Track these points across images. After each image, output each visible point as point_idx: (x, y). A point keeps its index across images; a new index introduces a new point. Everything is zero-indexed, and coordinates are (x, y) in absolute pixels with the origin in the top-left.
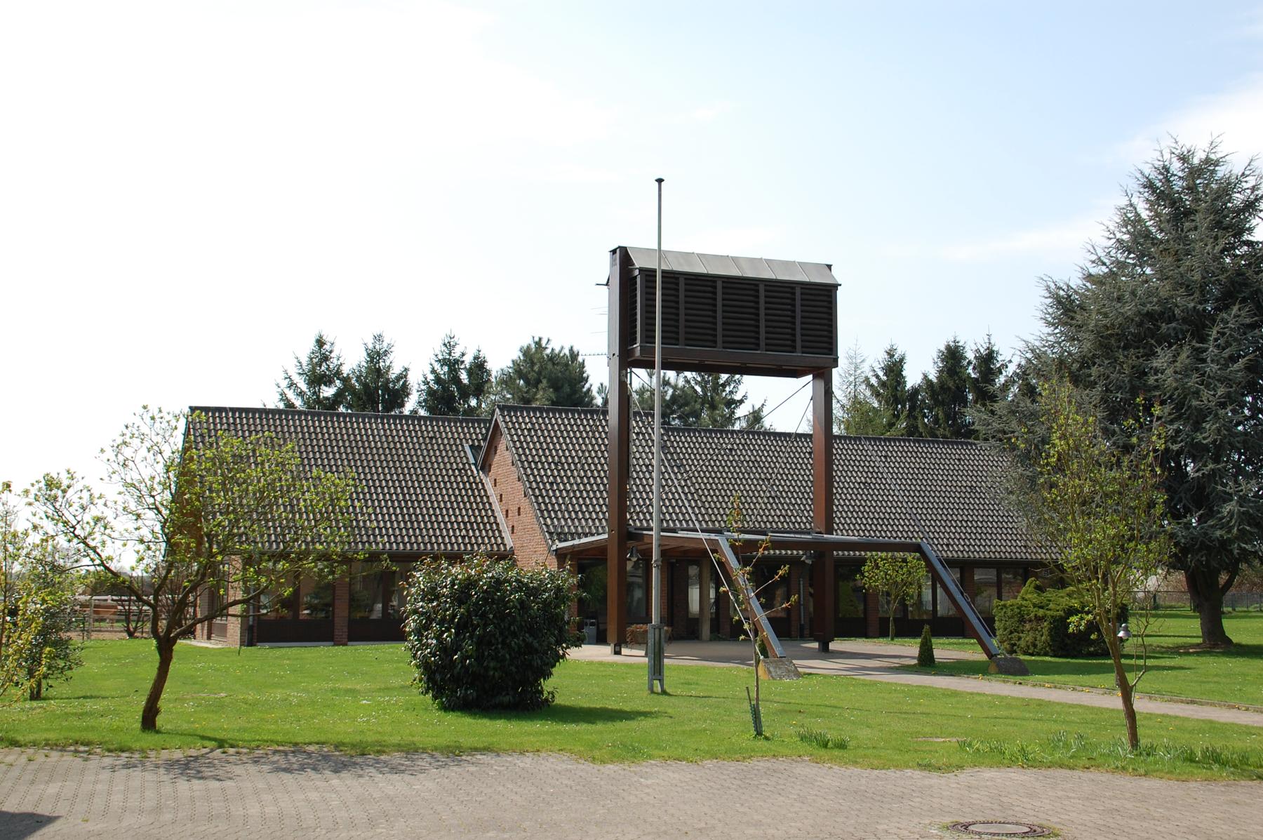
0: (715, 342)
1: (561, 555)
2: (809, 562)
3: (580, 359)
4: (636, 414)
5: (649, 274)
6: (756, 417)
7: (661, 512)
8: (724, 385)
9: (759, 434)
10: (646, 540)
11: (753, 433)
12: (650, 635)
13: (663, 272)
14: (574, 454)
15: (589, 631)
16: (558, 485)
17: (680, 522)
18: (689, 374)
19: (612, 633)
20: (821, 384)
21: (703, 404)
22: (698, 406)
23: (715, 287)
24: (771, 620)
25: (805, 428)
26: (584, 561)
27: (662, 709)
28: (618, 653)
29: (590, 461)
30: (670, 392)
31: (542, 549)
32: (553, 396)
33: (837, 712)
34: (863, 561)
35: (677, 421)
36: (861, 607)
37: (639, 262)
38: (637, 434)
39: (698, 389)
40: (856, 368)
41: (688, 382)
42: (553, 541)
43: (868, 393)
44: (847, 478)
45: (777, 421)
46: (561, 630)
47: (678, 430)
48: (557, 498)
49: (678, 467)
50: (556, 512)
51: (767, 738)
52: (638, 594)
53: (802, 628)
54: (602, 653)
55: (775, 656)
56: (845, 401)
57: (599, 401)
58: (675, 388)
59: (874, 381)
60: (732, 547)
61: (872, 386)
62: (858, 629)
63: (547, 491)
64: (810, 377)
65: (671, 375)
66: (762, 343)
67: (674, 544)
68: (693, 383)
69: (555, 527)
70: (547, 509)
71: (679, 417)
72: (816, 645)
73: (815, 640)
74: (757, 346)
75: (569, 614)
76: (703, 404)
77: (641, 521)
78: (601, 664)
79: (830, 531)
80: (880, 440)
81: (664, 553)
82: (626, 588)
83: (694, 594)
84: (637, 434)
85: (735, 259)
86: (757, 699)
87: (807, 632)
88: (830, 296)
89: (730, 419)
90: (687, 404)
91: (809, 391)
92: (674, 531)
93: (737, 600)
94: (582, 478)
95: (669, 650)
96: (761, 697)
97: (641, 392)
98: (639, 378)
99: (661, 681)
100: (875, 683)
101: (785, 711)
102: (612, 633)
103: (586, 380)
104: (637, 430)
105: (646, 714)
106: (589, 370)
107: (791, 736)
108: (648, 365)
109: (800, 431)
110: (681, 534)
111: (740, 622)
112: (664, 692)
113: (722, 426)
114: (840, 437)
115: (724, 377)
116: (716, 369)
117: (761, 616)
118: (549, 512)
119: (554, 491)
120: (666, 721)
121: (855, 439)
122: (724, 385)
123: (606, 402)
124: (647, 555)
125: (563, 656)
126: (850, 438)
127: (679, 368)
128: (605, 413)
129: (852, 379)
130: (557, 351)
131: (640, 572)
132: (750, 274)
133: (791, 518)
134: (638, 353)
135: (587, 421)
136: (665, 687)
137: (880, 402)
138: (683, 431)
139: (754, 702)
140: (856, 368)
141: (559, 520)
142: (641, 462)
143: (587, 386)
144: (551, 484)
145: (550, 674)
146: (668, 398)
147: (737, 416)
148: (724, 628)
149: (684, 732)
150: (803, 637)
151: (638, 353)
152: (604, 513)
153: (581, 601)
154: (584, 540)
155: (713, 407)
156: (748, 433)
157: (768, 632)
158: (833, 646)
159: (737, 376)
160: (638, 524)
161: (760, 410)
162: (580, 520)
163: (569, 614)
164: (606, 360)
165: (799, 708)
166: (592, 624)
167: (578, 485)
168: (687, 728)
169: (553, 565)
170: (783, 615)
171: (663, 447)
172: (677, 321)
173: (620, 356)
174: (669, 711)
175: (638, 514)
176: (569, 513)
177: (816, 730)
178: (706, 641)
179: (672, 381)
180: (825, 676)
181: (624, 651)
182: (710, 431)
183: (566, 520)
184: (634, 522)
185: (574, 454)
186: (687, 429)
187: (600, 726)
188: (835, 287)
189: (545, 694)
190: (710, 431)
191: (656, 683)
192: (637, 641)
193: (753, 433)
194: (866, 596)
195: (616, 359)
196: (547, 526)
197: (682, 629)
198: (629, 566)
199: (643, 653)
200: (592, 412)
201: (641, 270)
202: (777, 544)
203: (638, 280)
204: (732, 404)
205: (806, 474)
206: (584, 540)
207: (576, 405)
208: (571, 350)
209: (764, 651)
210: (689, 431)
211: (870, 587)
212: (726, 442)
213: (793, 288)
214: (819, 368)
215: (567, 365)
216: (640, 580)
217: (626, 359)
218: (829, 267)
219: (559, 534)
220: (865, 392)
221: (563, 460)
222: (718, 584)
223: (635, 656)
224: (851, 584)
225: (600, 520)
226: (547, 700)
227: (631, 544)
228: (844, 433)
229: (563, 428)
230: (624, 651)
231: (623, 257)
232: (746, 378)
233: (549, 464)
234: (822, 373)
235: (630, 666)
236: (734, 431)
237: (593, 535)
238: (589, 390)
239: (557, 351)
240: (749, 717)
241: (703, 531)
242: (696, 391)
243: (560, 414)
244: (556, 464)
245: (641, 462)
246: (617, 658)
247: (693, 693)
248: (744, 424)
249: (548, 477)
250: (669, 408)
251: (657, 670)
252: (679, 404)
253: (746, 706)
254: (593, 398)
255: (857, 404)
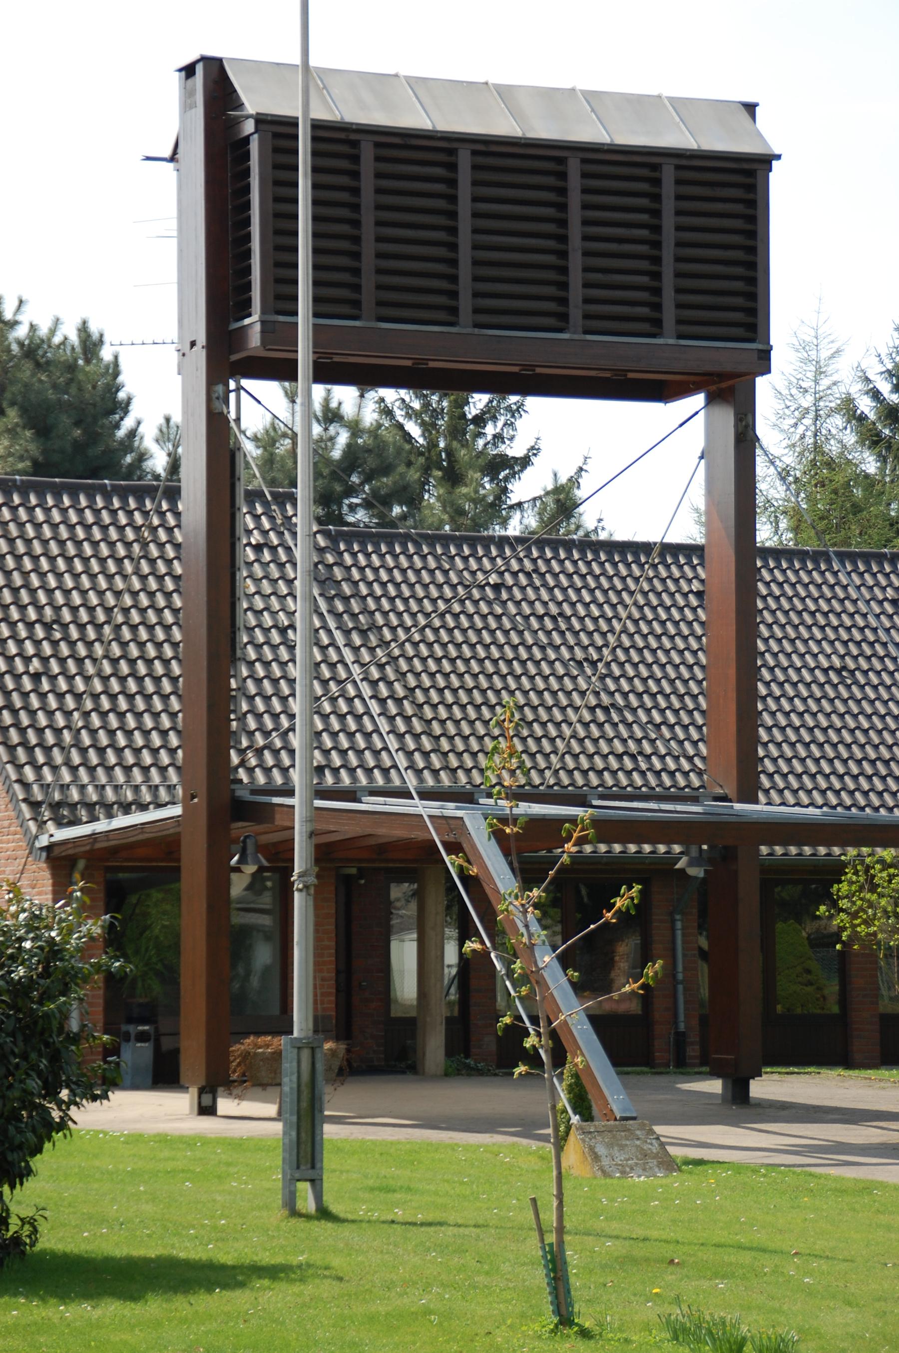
0: (454, 311)
1: (61, 861)
2: (697, 872)
3: (106, 354)
4: (254, 496)
5: (278, 130)
6: (563, 502)
7: (329, 737)
8: (480, 420)
9: (569, 545)
10: (280, 820)
11: (555, 545)
12: (288, 1065)
13: (317, 126)
14: (94, 599)
15: (136, 1055)
16: (53, 678)
17: (369, 771)
18: (390, 395)
19: (193, 1060)
20: (726, 417)
21: (426, 470)
22: (414, 475)
23: (453, 167)
24: (598, 1021)
25: (687, 531)
26: (120, 877)
27: (317, 1258)
28: (207, 1110)
29: (135, 617)
30: (343, 438)
31: (12, 844)
32: (34, 449)
33: (768, 1263)
34: (836, 871)
35: (361, 515)
36: (833, 988)
37: (254, 101)
38: (258, 548)
39: (414, 429)
40: (819, 372)
41: (388, 412)
42: (41, 825)
43: (850, 438)
44: (791, 656)
45: (619, 512)
46: (55, 1058)
47: (362, 536)
48: (50, 714)
49: (363, 633)
50: (47, 750)
51: (585, 1334)
52: (263, 955)
53: (680, 1040)
54: (164, 1112)
55: (609, 1115)
56: (789, 459)
57: (158, 462)
58: (355, 428)
59: (866, 405)
60: (498, 835)
61: (862, 418)
62: (824, 1044)
63: (25, 695)
64: (698, 400)
65: (345, 396)
66: (576, 312)
67: (349, 830)
68: (399, 415)
69: (45, 787)
70: (24, 744)
71: (367, 505)
72: (715, 1086)
73: (715, 1073)
74: (562, 321)
75: (80, 1011)
76: (426, 470)
77: (267, 771)
78: (164, 1140)
79: (749, 794)
80: (880, 558)
81: (325, 853)
82: (229, 943)
83: (404, 954)
84: (258, 548)
85: (505, 93)
86: (561, 1230)
87: (693, 1051)
88: (751, 188)
89: (497, 507)
90: (386, 469)
91: (695, 436)
92: (351, 795)
93: (510, 973)
94: (114, 662)
95: (336, 1101)
96: (568, 1225)
97: (268, 440)
98: (260, 405)
99: (316, 1183)
100: (867, 1188)
101: (635, 1261)
102: (193, 1060)
103: (125, 407)
104: (256, 538)
105: (274, 1272)
106: (131, 382)
107: (647, 1328)
108: (281, 369)
109: (674, 538)
110: (370, 804)
111: (517, 1032)
112: (324, 1213)
113: (475, 528)
114: (777, 553)
115: (479, 401)
116: (462, 382)
117: (573, 1014)
118: (30, 750)
119: (43, 696)
120: (326, 1288)
121: (816, 557)
122: (480, 420)
123: (174, 466)
124: (279, 857)
125: (62, 1126)
126: (803, 555)
127: (366, 377)
128: (173, 494)
129: (807, 401)
130: (43, 331)
131: (266, 900)
132: (544, 128)
133: (656, 762)
134: (255, 339)
135: (128, 515)
136: (329, 1200)
137: (883, 459)
138: (376, 539)
139: (551, 1238)
140: (819, 372)
141: (55, 769)
142: (268, 620)
143: (128, 423)
144: (36, 677)
145: (29, 1172)
146: (336, 454)
147: (513, 499)
148: (480, 1041)
149: (372, 1319)
150: (682, 1063)
151: (255, 339)
152: (172, 752)
153: (111, 979)
154: (121, 821)
155: (453, 477)
156: (541, 544)
157: (589, 1053)
158: (761, 1088)
159: (513, 399)
160: (261, 778)
161: (574, 482)
162: (109, 769)
163: (80, 1011)
164: (174, 357)
165: (668, 1251)
166: (142, 1037)
167: (105, 679)
168: (381, 1308)
169: (39, 890)
170: (634, 1007)
171: (324, 580)
172: (357, 256)
173: (211, 347)
174: (336, 1262)
175: (259, 752)
176: (83, 751)
177: (712, 1312)
178: (435, 1078)
179: (348, 410)
180: (738, 1168)
181: (225, 1105)
182: (445, 540)
183: (74, 769)
184: (250, 776)
185: (94, 599)
186: (386, 535)
187: (154, 1307)
188: (766, 161)
189: (14, 1224)
190: (445, 540)
191: (304, 1188)
192: (256, 1078)
193: (555, 545)
194: (846, 962)
195: (200, 356)
196: (26, 786)
197: (373, 1044)
198: (238, 885)
199: (271, 1109)
200: (141, 493)
201: (262, 121)
202: (606, 829)
203: (254, 147)
204: (504, 467)
205: (691, 649)
206: (121, 821)
207: (94, 474)
208: (83, 330)
209: (582, 1102)
210: (390, 540)
211: (855, 936)
212: (486, 568)
213: (355, 144)
214: (722, 376)
215: (72, 367)
216: (266, 921)
217: (227, 357)
218: (750, 108)
219: (55, 807)
220: (842, 436)
221: (67, 616)
222: (466, 932)
223: (253, 1119)
224: (810, 927)
225: (163, 770)
226: (16, 1240)
227: (240, 829)
228: (788, 539)
229: (64, 533)
230: (225, 1105)
231: (214, 83)
232: (533, 403)
233: (30, 625)
234: (732, 390)
235: (236, 1144)
236: (504, 541)
237: (143, 807)
238: (132, 433)
239: (43, 331)
240: (539, 1278)
241: (425, 795)
242: (407, 437)
243: (41, 497)
244: (48, 627)
245: (268, 620)
246: (206, 1124)
247: (399, 1214)
248: (532, 521)
249: (27, 660)
250: (334, 484)
251: (305, 1155)
252: (362, 473)
253: (532, 1248)
254: (142, 457)
255: (821, 469)
